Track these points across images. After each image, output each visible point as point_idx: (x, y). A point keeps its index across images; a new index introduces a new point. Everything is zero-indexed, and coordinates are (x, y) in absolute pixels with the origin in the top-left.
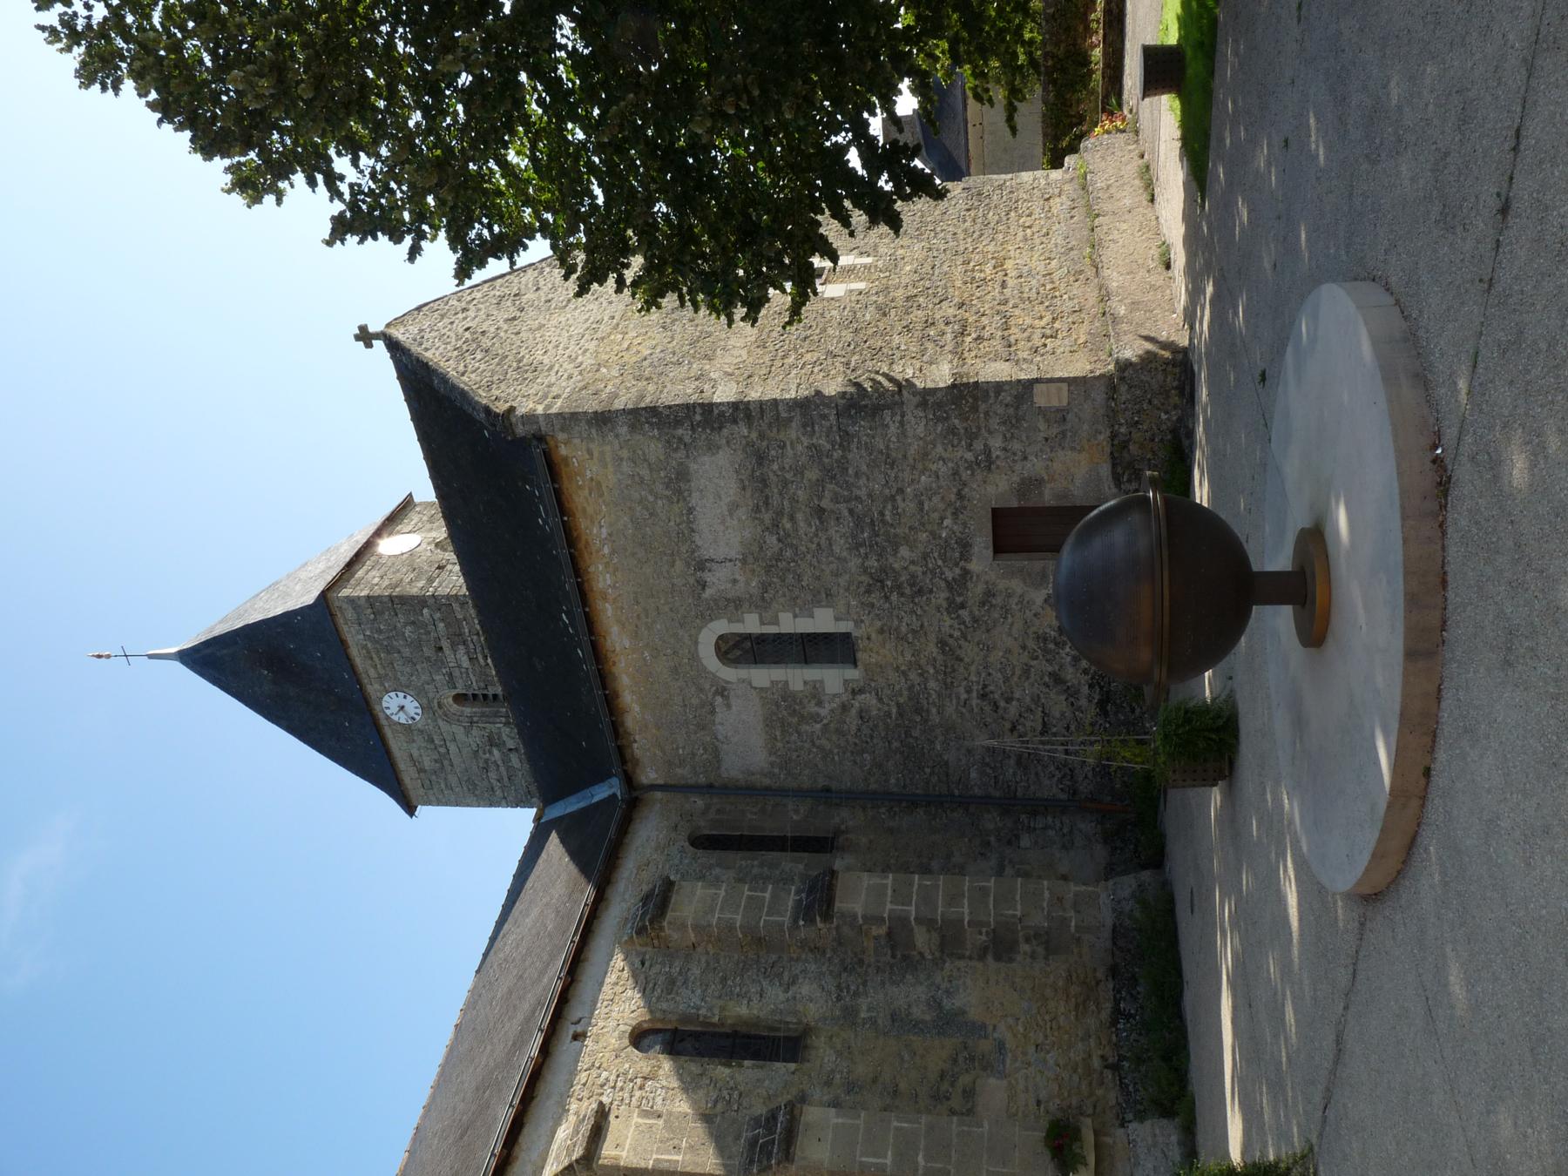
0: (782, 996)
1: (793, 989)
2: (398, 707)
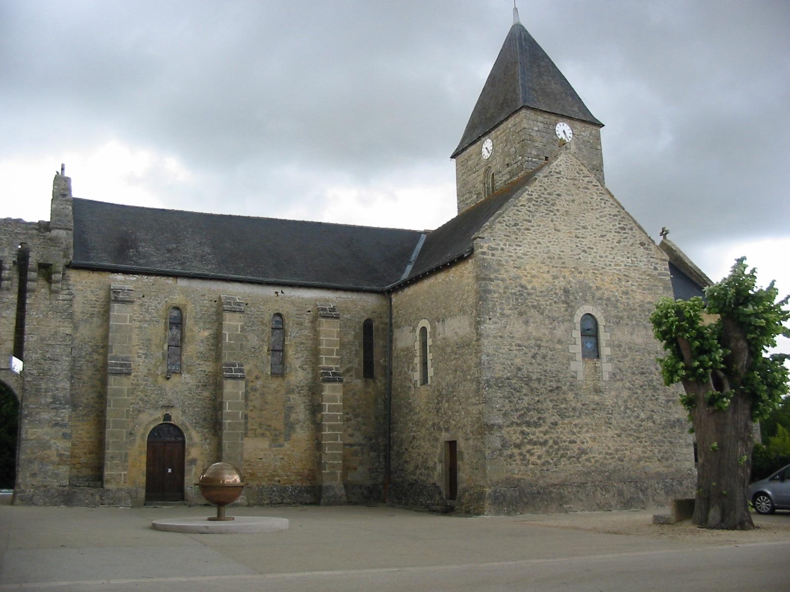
0: (297, 366)
1: (300, 370)
2: (488, 144)
